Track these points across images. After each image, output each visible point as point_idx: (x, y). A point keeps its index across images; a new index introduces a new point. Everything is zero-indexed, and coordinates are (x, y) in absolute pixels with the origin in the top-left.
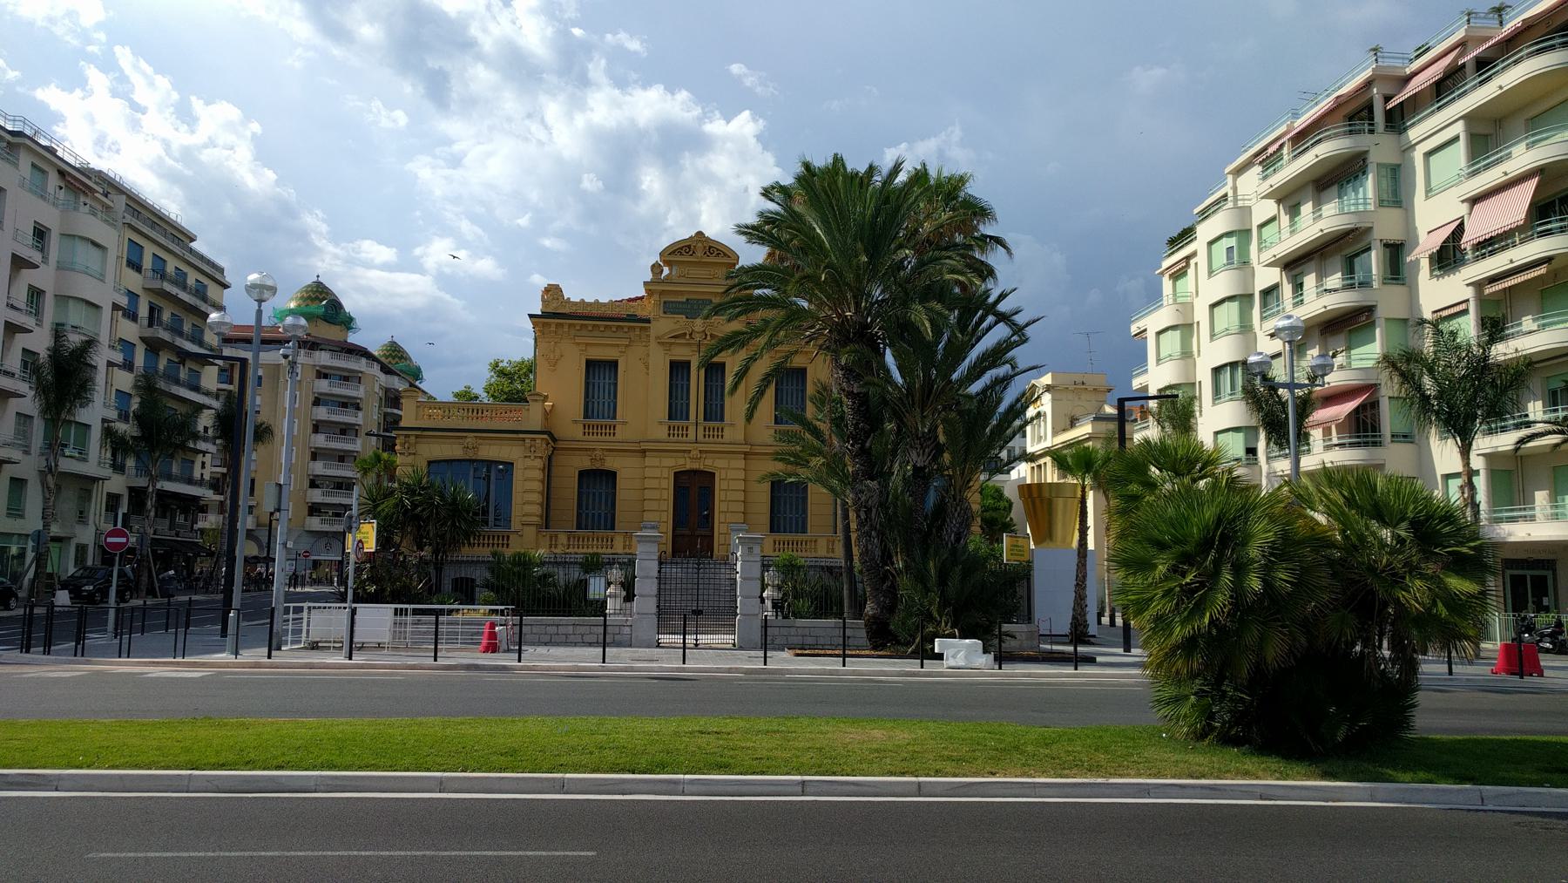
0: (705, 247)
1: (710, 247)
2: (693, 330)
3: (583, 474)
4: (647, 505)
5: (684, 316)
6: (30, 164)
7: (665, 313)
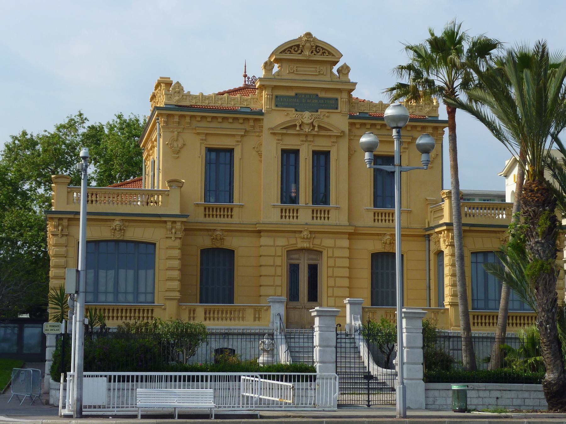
0: (312, 46)
1: (317, 47)
2: (302, 122)
3: (204, 252)
4: (263, 281)
5: (293, 109)
6: (491, 36)
7: (277, 106)
